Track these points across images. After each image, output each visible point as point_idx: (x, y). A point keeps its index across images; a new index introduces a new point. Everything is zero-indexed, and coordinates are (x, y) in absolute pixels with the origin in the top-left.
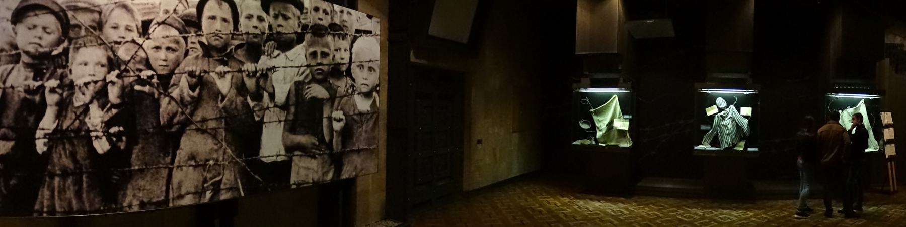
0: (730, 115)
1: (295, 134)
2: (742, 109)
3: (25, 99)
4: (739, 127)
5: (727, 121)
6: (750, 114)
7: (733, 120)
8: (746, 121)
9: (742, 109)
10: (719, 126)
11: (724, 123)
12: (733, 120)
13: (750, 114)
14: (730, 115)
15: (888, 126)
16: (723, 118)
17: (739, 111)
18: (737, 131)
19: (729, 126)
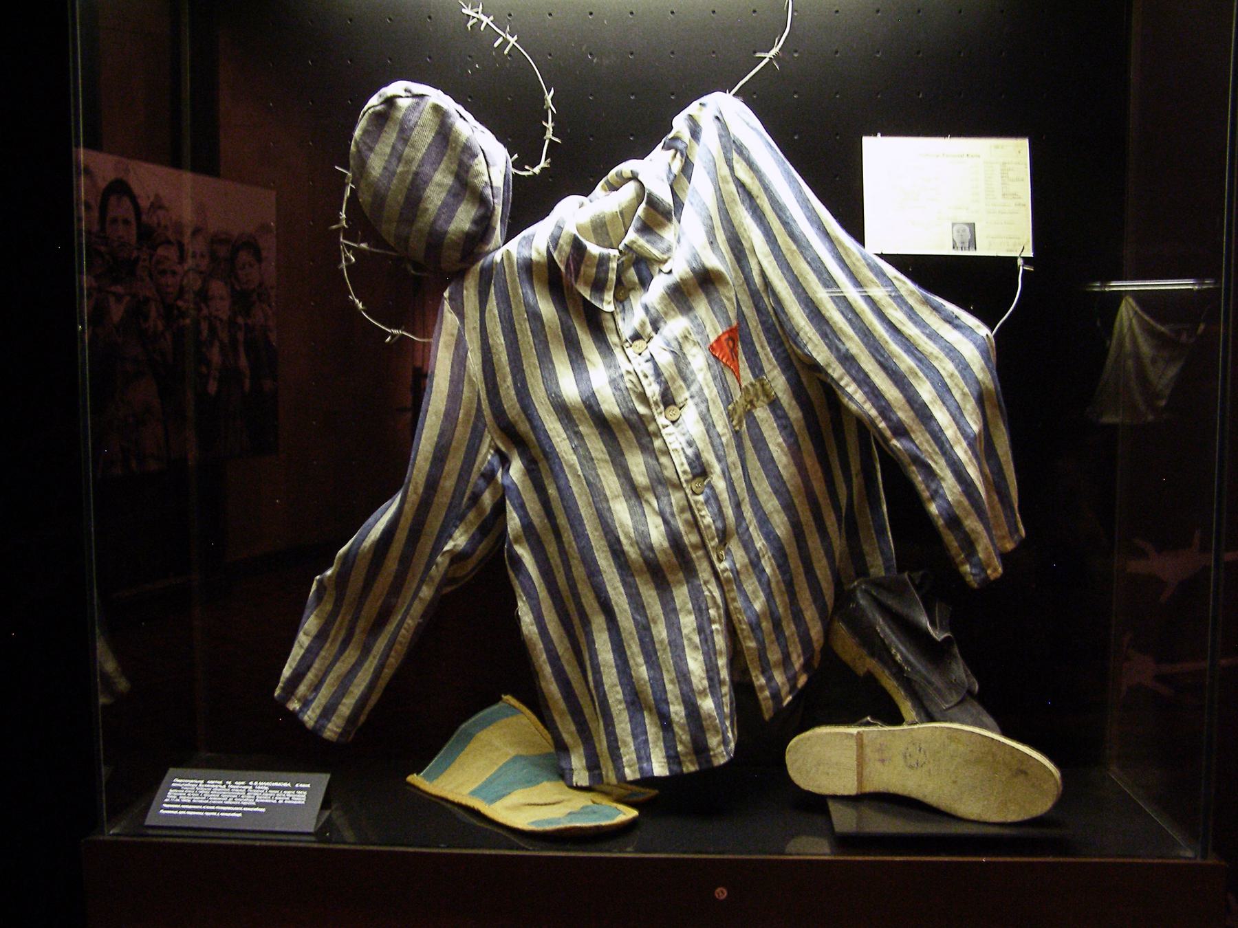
0: (687, 245)
1: (1108, 350)
2: (887, 160)
3: (85, 147)
4: (838, 443)
5: (657, 356)
6: (1007, 231)
7: (760, 331)
8: (960, 344)
9: (887, 160)
10: (522, 439)
11: (600, 379)
12: (760, 331)
13: (1007, 231)
14: (687, 245)
15: (703, 693)
16: (579, 293)
17: (844, 197)
18: (806, 507)
19: (683, 432)
